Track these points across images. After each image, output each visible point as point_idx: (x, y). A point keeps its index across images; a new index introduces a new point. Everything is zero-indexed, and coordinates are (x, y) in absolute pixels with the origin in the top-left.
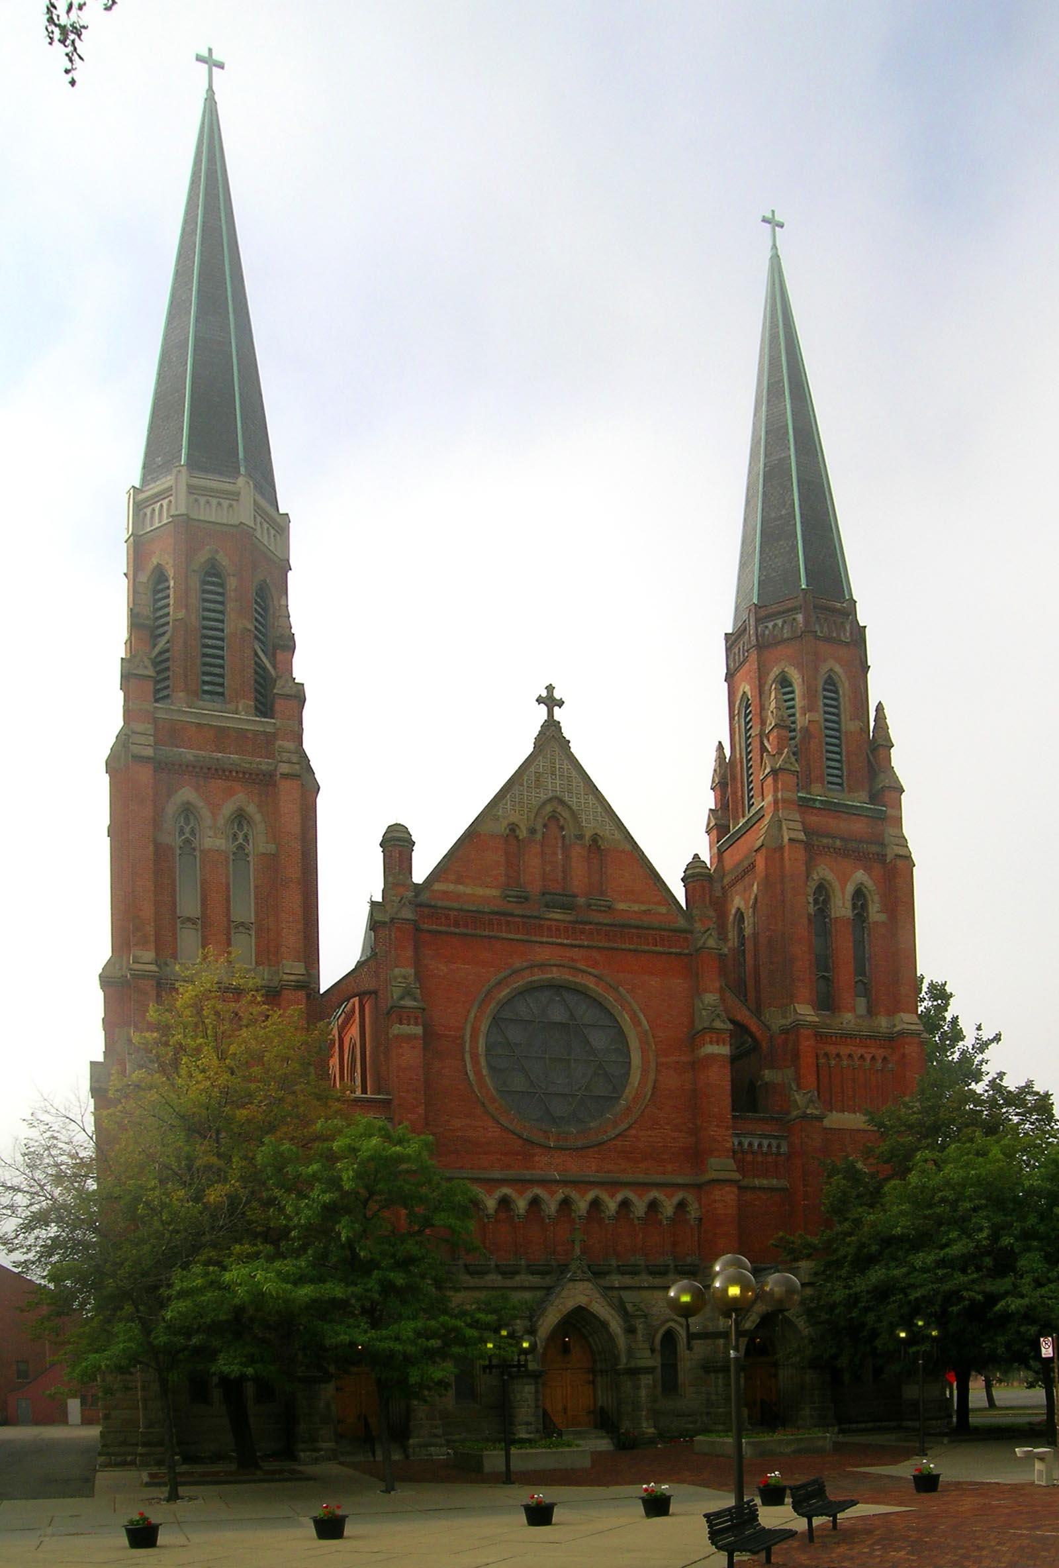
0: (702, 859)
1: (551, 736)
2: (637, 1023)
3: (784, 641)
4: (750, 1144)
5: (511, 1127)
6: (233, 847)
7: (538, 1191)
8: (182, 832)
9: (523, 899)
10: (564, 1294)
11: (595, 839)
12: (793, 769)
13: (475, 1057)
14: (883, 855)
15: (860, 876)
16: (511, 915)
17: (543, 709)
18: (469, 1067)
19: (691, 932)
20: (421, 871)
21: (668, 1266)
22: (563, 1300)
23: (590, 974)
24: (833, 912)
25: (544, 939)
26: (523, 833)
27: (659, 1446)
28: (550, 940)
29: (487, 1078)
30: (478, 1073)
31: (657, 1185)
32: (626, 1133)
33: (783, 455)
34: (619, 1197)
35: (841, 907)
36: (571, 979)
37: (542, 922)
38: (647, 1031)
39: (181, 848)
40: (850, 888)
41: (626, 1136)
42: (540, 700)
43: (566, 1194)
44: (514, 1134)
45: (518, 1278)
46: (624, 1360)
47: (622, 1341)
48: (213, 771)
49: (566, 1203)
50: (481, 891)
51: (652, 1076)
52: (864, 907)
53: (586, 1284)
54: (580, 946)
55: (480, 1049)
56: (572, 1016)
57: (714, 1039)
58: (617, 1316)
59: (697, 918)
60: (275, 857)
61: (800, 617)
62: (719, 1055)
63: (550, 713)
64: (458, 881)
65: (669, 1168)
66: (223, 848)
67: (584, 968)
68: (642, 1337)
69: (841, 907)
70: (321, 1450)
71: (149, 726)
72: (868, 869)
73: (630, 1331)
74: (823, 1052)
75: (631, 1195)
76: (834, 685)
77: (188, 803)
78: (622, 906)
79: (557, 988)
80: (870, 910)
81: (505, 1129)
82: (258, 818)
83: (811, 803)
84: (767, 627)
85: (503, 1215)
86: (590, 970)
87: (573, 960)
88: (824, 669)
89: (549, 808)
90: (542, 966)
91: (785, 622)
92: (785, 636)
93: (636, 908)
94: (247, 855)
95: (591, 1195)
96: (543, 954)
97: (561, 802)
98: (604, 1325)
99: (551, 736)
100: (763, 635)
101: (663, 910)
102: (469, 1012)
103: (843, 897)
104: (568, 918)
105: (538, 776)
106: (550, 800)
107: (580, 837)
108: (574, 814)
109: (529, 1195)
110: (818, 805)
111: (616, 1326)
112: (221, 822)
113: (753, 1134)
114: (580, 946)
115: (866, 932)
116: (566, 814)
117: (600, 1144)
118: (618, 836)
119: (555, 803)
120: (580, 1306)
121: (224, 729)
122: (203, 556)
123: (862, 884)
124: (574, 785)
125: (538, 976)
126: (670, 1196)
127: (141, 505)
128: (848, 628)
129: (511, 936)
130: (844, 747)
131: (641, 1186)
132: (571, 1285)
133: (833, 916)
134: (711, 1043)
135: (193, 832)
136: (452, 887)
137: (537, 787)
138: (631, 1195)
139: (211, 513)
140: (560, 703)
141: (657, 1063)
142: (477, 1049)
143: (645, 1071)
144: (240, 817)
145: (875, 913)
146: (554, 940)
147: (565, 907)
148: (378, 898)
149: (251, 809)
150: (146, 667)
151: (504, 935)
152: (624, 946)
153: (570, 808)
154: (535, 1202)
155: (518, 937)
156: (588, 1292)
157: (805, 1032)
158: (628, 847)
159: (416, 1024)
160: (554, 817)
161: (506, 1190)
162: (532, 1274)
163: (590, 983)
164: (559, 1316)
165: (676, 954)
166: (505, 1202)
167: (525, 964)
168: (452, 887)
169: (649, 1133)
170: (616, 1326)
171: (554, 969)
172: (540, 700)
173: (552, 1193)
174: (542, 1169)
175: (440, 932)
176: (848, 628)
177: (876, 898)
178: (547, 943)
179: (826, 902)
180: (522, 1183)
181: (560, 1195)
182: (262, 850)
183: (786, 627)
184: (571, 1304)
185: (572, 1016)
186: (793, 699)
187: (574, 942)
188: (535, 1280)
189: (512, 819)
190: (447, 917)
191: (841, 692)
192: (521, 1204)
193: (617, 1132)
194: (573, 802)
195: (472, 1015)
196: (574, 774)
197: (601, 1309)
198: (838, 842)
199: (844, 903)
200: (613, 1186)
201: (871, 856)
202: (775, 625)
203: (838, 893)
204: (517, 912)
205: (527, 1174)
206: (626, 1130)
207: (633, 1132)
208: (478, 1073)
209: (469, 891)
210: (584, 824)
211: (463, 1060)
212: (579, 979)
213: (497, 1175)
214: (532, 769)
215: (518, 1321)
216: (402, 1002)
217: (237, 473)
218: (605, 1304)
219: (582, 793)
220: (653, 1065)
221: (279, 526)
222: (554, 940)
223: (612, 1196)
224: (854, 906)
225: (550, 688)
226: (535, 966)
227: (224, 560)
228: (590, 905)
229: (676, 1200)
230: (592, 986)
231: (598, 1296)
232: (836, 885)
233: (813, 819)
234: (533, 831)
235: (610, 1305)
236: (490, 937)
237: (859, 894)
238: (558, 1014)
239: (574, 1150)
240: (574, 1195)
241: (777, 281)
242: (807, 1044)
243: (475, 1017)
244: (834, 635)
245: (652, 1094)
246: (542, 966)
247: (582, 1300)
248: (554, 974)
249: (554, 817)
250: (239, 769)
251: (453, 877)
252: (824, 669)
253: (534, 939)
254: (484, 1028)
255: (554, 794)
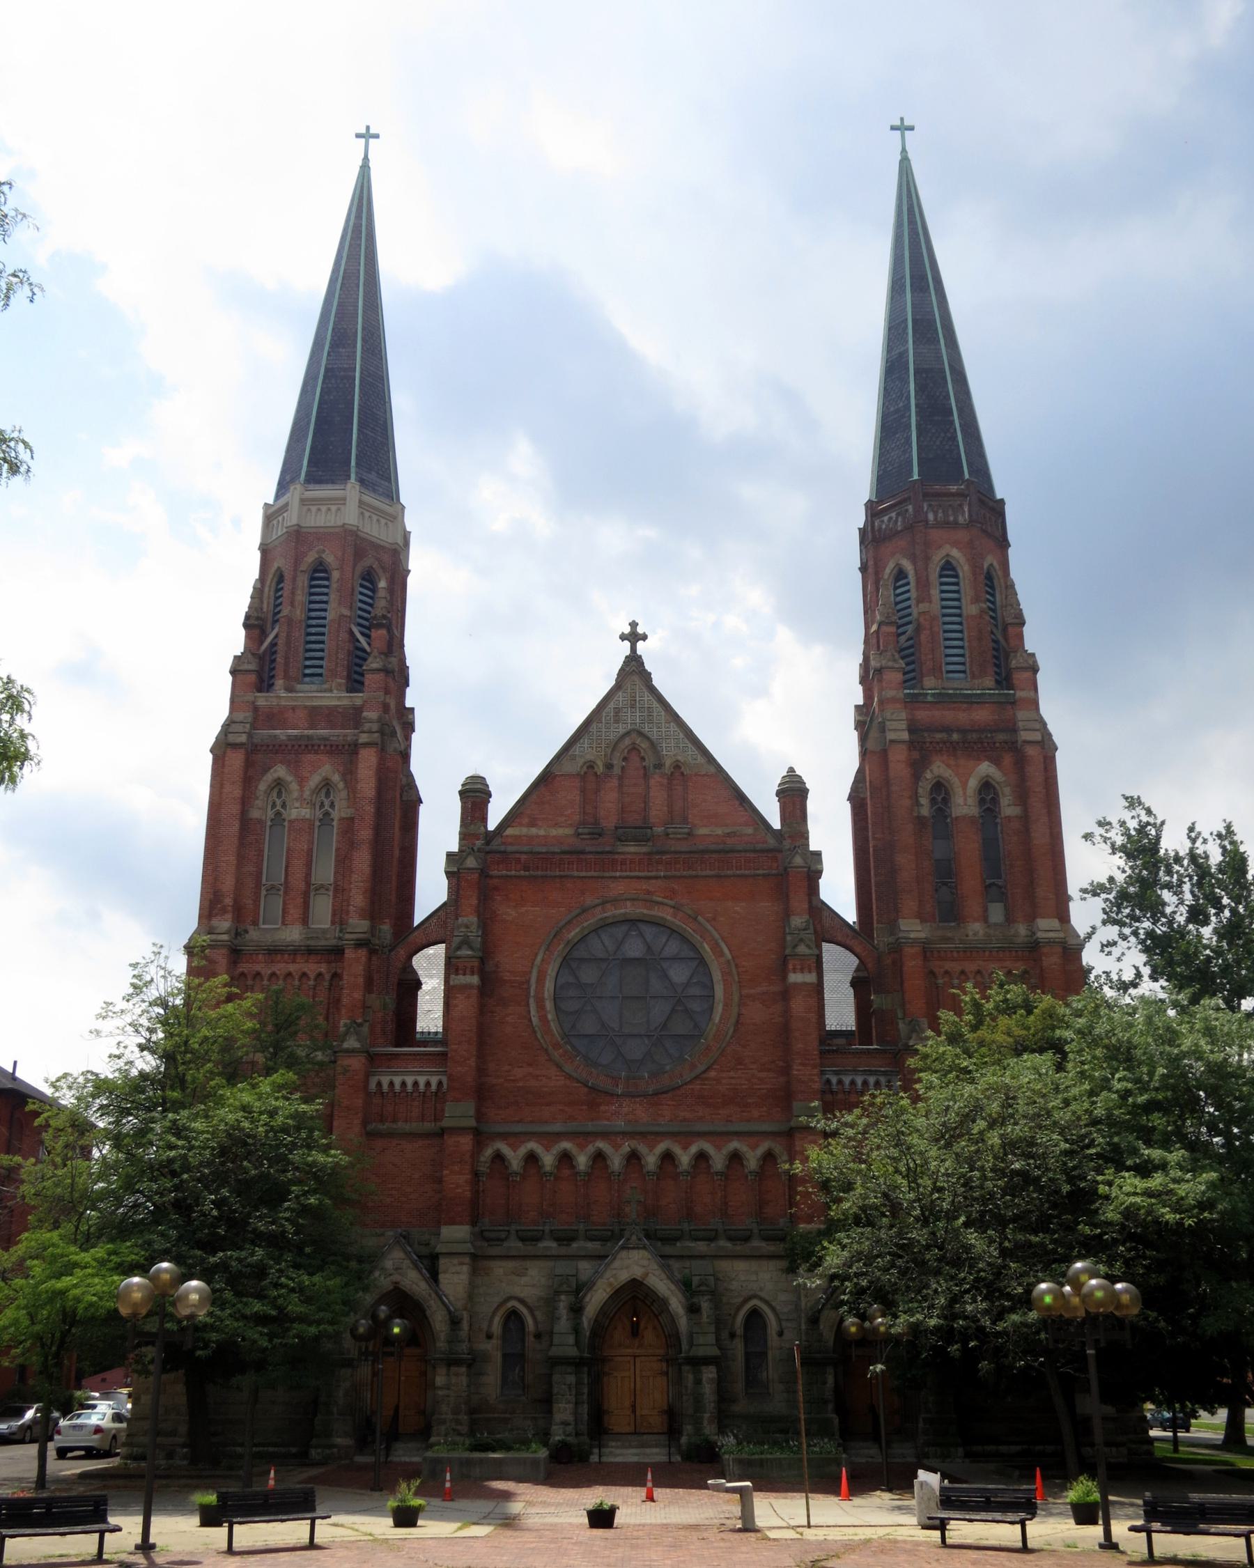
0: (797, 773)
1: (634, 670)
2: (719, 953)
3: (898, 533)
4: (853, 1083)
5: (575, 1075)
6: (319, 814)
7: (601, 1144)
8: (274, 805)
9: (598, 834)
10: (617, 1264)
11: (677, 766)
12: (897, 666)
13: (541, 1006)
14: (1013, 743)
15: (986, 768)
16: (582, 852)
17: (627, 644)
18: (533, 1012)
19: (780, 851)
20: (496, 814)
21: (751, 1230)
22: (614, 1272)
23: (666, 905)
24: (953, 810)
25: (618, 874)
26: (600, 769)
27: (879, 1367)
28: (625, 874)
29: (552, 1024)
30: (543, 1019)
31: (738, 1134)
32: (704, 1076)
33: (902, 349)
34: (694, 1149)
35: (964, 804)
36: (645, 911)
37: (616, 856)
38: (729, 961)
39: (272, 820)
40: (973, 783)
41: (706, 1079)
42: (623, 637)
43: (633, 1146)
44: (578, 1081)
45: (575, 1245)
46: (685, 1346)
47: (683, 1323)
48: (303, 747)
49: (634, 1157)
50: (554, 832)
51: (735, 1011)
52: (995, 801)
53: (643, 1253)
54: (656, 878)
55: (546, 993)
56: (649, 948)
57: (799, 967)
58: (677, 1292)
59: (786, 836)
60: (352, 819)
61: (910, 508)
62: (805, 984)
63: (633, 649)
64: (532, 824)
65: (756, 1113)
66: (308, 816)
67: (660, 899)
68: (708, 1317)
69: (964, 804)
70: (333, 1446)
71: (248, 714)
72: (997, 762)
73: (693, 1310)
74: (942, 970)
75: (708, 1147)
76: (954, 569)
77: (279, 779)
78: (703, 831)
79: (633, 922)
80: (1002, 805)
81: (569, 1077)
82: (341, 785)
83: (921, 698)
84: (883, 521)
85: (566, 1172)
86: (666, 901)
87: (649, 892)
88: (937, 558)
89: (627, 741)
90: (615, 901)
91: (898, 515)
92: (899, 529)
93: (719, 831)
94: (333, 820)
95: (661, 1147)
96: (618, 889)
97: (640, 734)
98: (664, 1303)
99: (634, 670)
100: (880, 529)
101: (750, 831)
102: (536, 955)
103: (965, 793)
104: (644, 849)
105: (617, 711)
106: (628, 733)
107: (659, 766)
108: (653, 745)
109: (591, 1149)
110: (929, 699)
111: (676, 1304)
112: (307, 793)
113: (855, 1071)
114: (656, 878)
115: (999, 828)
116: (645, 745)
117: (674, 1089)
118: (701, 760)
119: (634, 735)
120: (634, 1279)
121: (314, 708)
122: (311, 558)
123: (987, 776)
124: (655, 714)
125: (612, 912)
126: (754, 1147)
127: (271, 516)
128: (966, 510)
129: (583, 874)
130: (966, 633)
131: (719, 1136)
132: (624, 1254)
133: (954, 816)
134: (794, 971)
135: (284, 805)
136: (524, 831)
137: (617, 721)
138: (708, 1147)
139: (320, 519)
140: (644, 637)
141: (741, 996)
142: (543, 993)
143: (727, 1005)
144: (327, 786)
145: (1008, 808)
146: (628, 873)
147: (637, 840)
148: (455, 848)
149: (336, 778)
150: (249, 663)
151: (576, 873)
152: (704, 873)
153: (648, 738)
154: (599, 1157)
155: (589, 874)
156: (645, 1263)
157: (908, 951)
158: (712, 770)
159: (472, 973)
160: (634, 748)
161: (566, 1145)
162: (591, 1240)
163: (666, 914)
164: (610, 1291)
165: (764, 875)
166: (565, 1158)
167: (597, 901)
168: (524, 831)
169: (732, 1074)
170: (676, 1304)
171: (628, 903)
172: (623, 637)
173: (617, 1147)
174: (608, 1119)
175: (511, 877)
176: (966, 510)
177: (1007, 790)
178: (620, 877)
179: (946, 801)
180: (583, 1137)
181: (626, 1148)
182: (344, 815)
183: (900, 519)
184: (624, 1277)
185: (649, 948)
186: (908, 591)
187: (650, 874)
188: (592, 1246)
189: (589, 757)
190: (518, 860)
191: (961, 575)
192: (582, 1161)
193: (693, 1075)
194: (654, 734)
195: (539, 958)
196: (655, 704)
197: (661, 1284)
198: (955, 737)
199: (965, 800)
200: (686, 1137)
201: (998, 745)
202: (891, 518)
203: (959, 791)
204: (588, 849)
205: (590, 1127)
206: (704, 1072)
207: (712, 1074)
208: (543, 1019)
209: (542, 832)
210: (664, 753)
211: (528, 1005)
212: (657, 912)
213: (557, 1127)
214: (612, 705)
215: (563, 1297)
216: (459, 953)
217: (349, 477)
218: (663, 1276)
219: (663, 721)
220: (736, 998)
221: (390, 515)
222: (628, 873)
223: (685, 1148)
224: (982, 801)
225: (634, 625)
226: (607, 902)
227: (329, 559)
228: (668, 834)
229: (760, 1151)
230: (669, 918)
231: (656, 1267)
232: (956, 782)
233: (923, 715)
234: (609, 766)
235: (669, 1278)
236: (561, 877)
237: (986, 786)
238: (634, 949)
239: (645, 1096)
240: (642, 1149)
241: (905, 184)
242: (912, 964)
243: (543, 960)
244: (951, 518)
245: (735, 1031)
246: (615, 901)
247: (637, 1272)
248: (629, 909)
249: (634, 748)
250: (327, 743)
251: (526, 820)
252: (937, 558)
253: (607, 874)
254: (552, 971)
255: (633, 727)
